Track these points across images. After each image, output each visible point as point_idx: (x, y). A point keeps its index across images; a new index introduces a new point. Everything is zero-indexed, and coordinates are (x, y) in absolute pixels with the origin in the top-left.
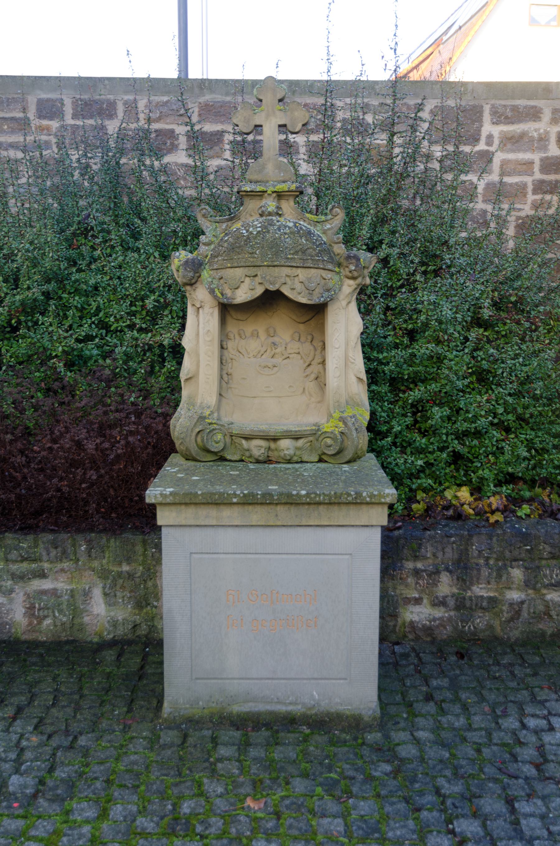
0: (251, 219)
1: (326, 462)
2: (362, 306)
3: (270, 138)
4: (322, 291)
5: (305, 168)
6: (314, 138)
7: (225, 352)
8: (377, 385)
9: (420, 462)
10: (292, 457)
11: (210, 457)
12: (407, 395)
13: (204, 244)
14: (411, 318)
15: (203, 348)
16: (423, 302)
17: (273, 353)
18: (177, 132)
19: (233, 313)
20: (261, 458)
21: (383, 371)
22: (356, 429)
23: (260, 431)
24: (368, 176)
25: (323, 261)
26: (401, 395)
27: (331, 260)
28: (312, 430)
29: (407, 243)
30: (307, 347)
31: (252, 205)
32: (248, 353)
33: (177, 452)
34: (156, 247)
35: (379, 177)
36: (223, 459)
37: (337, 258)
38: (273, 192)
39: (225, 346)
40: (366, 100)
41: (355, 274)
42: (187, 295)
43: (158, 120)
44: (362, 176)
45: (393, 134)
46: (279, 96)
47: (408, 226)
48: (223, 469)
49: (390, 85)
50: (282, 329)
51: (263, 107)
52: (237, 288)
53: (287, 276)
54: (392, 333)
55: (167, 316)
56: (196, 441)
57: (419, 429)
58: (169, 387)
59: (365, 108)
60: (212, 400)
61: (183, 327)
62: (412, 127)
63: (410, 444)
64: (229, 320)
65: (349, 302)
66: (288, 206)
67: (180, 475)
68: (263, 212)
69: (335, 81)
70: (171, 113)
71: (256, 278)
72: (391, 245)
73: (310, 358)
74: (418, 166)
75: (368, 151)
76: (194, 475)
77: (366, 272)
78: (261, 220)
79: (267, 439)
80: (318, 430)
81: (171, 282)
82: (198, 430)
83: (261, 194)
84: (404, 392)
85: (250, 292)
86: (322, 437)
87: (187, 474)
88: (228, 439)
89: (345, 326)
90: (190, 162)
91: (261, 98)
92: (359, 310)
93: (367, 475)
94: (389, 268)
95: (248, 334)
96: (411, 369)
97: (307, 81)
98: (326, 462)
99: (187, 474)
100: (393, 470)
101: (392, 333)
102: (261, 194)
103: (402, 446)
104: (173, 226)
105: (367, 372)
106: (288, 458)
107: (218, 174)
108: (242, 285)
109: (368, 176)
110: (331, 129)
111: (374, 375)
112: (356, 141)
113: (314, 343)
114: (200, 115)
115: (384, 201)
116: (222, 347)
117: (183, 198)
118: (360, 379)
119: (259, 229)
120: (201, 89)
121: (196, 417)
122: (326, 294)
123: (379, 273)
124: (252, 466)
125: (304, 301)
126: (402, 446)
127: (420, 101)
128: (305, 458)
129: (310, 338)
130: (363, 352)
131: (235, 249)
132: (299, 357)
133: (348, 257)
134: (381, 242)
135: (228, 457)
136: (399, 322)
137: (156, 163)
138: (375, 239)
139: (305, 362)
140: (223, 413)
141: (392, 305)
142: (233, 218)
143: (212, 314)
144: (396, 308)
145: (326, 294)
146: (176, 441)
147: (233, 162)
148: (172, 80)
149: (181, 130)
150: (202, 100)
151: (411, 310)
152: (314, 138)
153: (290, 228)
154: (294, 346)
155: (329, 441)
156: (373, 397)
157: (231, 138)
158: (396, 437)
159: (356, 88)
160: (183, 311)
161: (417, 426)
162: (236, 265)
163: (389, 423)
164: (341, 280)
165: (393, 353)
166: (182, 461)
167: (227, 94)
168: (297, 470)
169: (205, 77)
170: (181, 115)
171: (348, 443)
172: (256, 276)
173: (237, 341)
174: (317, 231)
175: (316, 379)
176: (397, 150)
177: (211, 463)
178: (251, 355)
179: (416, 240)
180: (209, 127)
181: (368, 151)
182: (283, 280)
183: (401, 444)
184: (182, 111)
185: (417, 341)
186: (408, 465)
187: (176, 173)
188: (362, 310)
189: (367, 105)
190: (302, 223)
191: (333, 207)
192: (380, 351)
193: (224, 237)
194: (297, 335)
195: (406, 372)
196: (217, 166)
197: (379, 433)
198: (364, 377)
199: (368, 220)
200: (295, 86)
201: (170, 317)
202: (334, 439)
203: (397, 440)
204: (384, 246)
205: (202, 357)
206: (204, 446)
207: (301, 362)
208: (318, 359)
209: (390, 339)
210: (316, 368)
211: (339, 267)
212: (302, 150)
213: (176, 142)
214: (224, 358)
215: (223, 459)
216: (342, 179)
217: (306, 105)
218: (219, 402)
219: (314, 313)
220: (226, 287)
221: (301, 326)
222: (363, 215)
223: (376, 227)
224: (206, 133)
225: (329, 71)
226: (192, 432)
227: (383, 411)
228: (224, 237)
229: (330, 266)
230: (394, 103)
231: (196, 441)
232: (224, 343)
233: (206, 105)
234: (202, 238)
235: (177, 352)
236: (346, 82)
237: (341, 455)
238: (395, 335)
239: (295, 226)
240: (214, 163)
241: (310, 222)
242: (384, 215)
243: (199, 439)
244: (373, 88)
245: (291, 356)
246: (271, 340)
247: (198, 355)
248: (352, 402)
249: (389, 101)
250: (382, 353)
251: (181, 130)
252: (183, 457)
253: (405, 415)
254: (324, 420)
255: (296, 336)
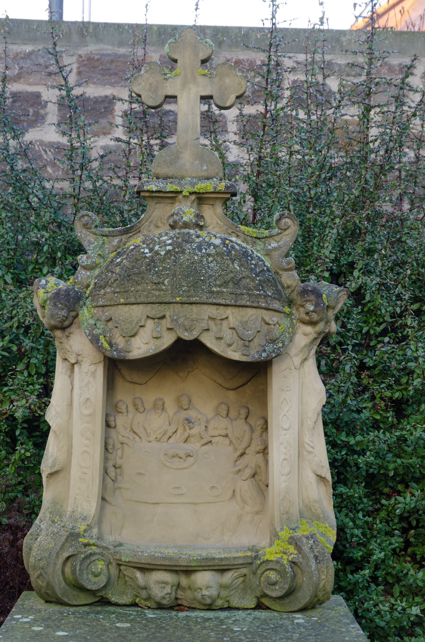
0: (157, 232)
1: (268, 608)
2: (323, 362)
3: (188, 111)
4: (263, 342)
5: (235, 154)
6: (250, 110)
7: (112, 432)
8: (345, 485)
9: (415, 610)
10: (214, 601)
11: (84, 599)
12: (392, 501)
13: (85, 268)
14: (398, 382)
15: (78, 426)
16: (416, 359)
17: (186, 435)
18: (45, 97)
19: (125, 372)
20: (165, 602)
21: (356, 464)
22: (316, 557)
23: (165, 558)
24: (331, 168)
25: (266, 296)
26: (384, 502)
27: (278, 295)
28: (245, 557)
29: (392, 269)
30: (239, 428)
31: (158, 212)
32: (148, 435)
33: (31, 588)
34: (8, 267)
35: (348, 170)
36: (104, 602)
37: (287, 292)
38: (191, 193)
39: (112, 423)
40: (327, 58)
41: (315, 317)
42: (57, 343)
43: (18, 78)
44: (322, 168)
45: (368, 108)
46: (203, 56)
47: (392, 244)
48: (105, 618)
49: (364, 38)
50: (202, 399)
51: (178, 71)
52: (133, 336)
53: (210, 318)
54: (370, 405)
55: (22, 372)
56: (63, 572)
57: (413, 556)
58: (20, 483)
59: (327, 69)
60: (89, 506)
61: (47, 391)
62: (397, 98)
63: (398, 580)
64: (120, 383)
65: (305, 360)
66: (213, 215)
67: (36, 629)
68: (175, 222)
69: (282, 30)
70: (36, 68)
71: (164, 321)
72: (367, 272)
73: (244, 444)
74: (406, 154)
75: (332, 131)
76: (59, 628)
77: (331, 314)
78: (172, 233)
79: (176, 572)
80: (256, 557)
81: (29, 320)
82: (66, 555)
83: (173, 196)
84: (388, 497)
85: (153, 341)
86: (262, 569)
87: (48, 626)
88: (114, 570)
89: (299, 395)
90: (64, 140)
91: (175, 57)
92: (319, 367)
93: (334, 631)
94: (364, 305)
95: (148, 405)
96: (399, 461)
97: (240, 28)
98: (268, 608)
99: (48, 626)
100: (372, 621)
101: (370, 405)
102: (173, 196)
103: (387, 583)
104: (34, 236)
105: (332, 464)
106: (208, 601)
107: (105, 159)
108: (142, 331)
109: (331, 168)
110: (277, 98)
111: (341, 469)
112: (314, 117)
113: (251, 420)
114: (79, 73)
115: (356, 206)
116: (108, 425)
117: (51, 195)
118: (321, 478)
119: (169, 248)
120: (83, 36)
121: (64, 534)
122: (269, 348)
123: (349, 312)
124: (150, 614)
125: (236, 356)
126: (387, 583)
127: (407, 61)
128: (235, 603)
129: (243, 412)
130: (326, 434)
131: (132, 278)
132: (227, 441)
133: (304, 292)
134: (351, 266)
135: (113, 599)
136: (382, 390)
137: (12, 143)
138: (343, 261)
139: (236, 449)
140: (106, 528)
141: (369, 362)
142: (129, 231)
143: (94, 374)
144: (375, 367)
145: (269, 348)
146: (30, 572)
147: (129, 143)
148: (40, 23)
149: (50, 95)
150: (83, 51)
151: (399, 370)
152: (250, 110)
153: (215, 247)
154: (220, 425)
155: (273, 576)
156: (341, 504)
157: (126, 106)
158: (377, 568)
159: (315, 39)
160: (46, 364)
161: (409, 550)
162: (132, 300)
163: (365, 546)
164: (293, 326)
165: (372, 436)
166: (40, 604)
167: (121, 44)
168: (222, 622)
169: (86, 20)
170: (50, 74)
171: (303, 579)
172: (163, 317)
173: (130, 416)
174: (257, 251)
175: (253, 476)
176: (374, 132)
177: (86, 609)
178: (152, 438)
179: (404, 263)
180: (93, 91)
181: (332, 131)
182: (204, 325)
183: (385, 579)
184: (54, 68)
185: (408, 416)
186: (396, 614)
187: (41, 156)
188: (323, 368)
189: (330, 64)
190: (234, 239)
191: (282, 217)
192: (351, 433)
193: (116, 257)
194: (224, 407)
195: (392, 466)
196: (104, 148)
197: (350, 561)
198: (327, 473)
199: (333, 233)
200: (222, 35)
201: (26, 373)
202: (281, 573)
203: (378, 573)
204: (356, 273)
205: (77, 439)
206: (76, 580)
207: (230, 449)
208: (256, 446)
209: (366, 414)
210: (252, 459)
211: (289, 306)
212: (233, 127)
213: (42, 112)
214: (111, 442)
215: (104, 602)
216: (293, 173)
217: (238, 62)
218: (101, 510)
219: (251, 376)
220: (117, 334)
221: (231, 395)
222: (324, 226)
223: (343, 243)
224: (88, 99)
225: (273, 17)
226: (57, 557)
227: (356, 526)
228: (116, 257)
229: (276, 305)
230: (370, 64)
231: (63, 572)
232: (112, 419)
233: (90, 59)
234: (82, 258)
235: (37, 431)
236: (297, 32)
237: (292, 598)
238: (374, 406)
239: (224, 243)
240: (99, 144)
241: (246, 237)
242: (355, 224)
243: (68, 570)
244: (338, 40)
245: (214, 440)
246: (184, 414)
247: (70, 437)
248: (308, 514)
249: (361, 59)
250: (354, 435)
251: (50, 95)
252: (42, 597)
253: (389, 534)
254: (264, 542)
255: (223, 410)
